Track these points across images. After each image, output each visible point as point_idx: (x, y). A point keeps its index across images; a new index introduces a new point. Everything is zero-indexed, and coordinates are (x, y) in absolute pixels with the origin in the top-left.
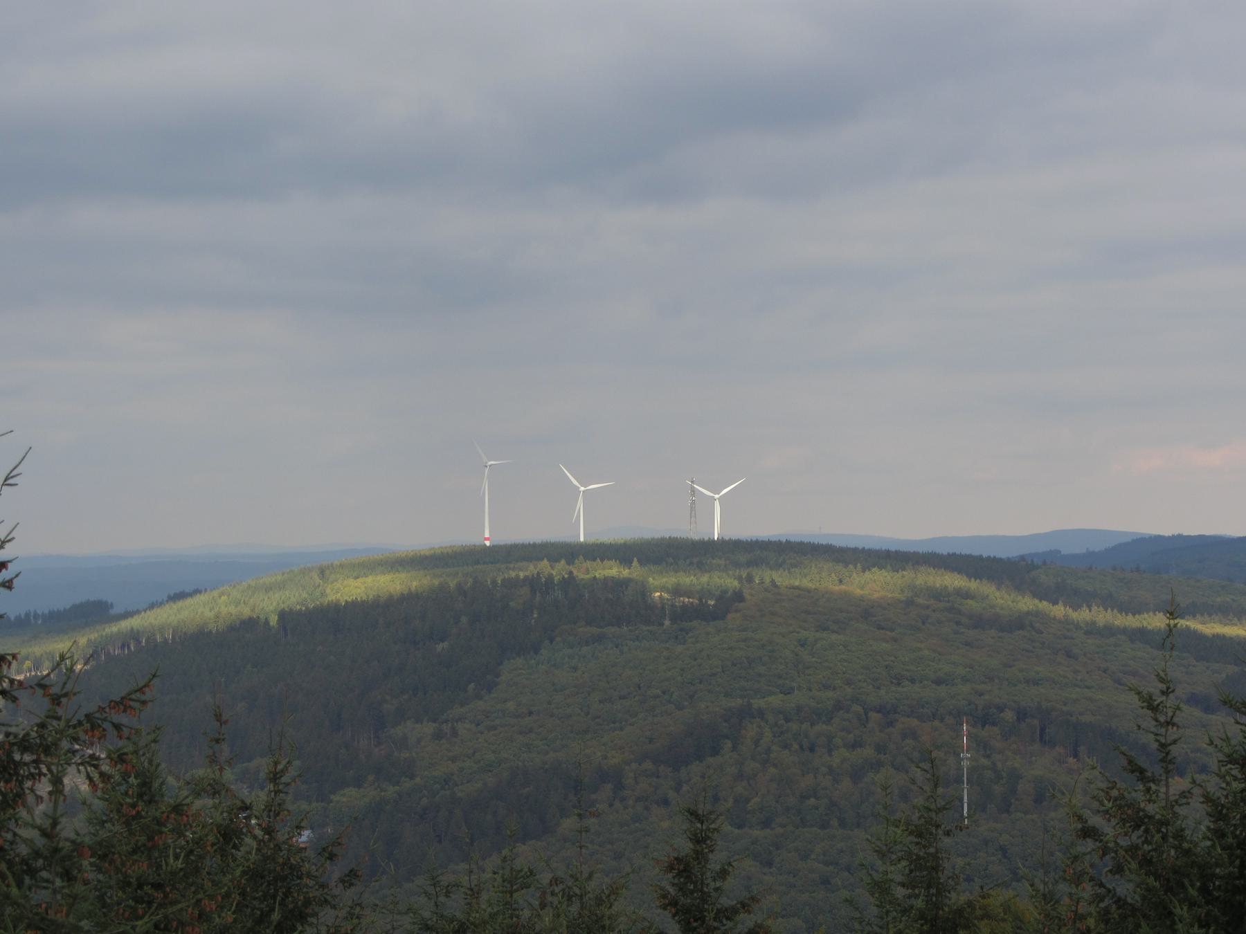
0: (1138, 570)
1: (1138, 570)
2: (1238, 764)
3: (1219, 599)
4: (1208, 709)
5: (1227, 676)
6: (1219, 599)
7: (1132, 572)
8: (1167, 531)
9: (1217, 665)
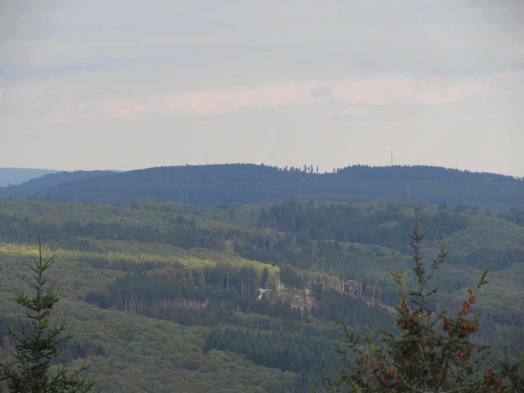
0: (48, 198)
1: (48, 198)
2: (30, 348)
3: (110, 220)
4: (103, 305)
5: (117, 279)
6: (110, 220)
7: (43, 200)
8: (71, 169)
9: (109, 271)
